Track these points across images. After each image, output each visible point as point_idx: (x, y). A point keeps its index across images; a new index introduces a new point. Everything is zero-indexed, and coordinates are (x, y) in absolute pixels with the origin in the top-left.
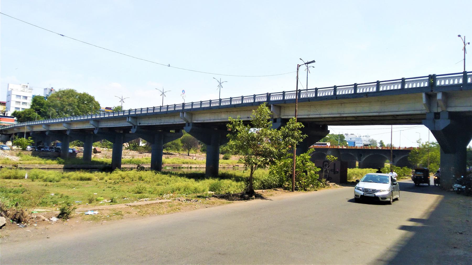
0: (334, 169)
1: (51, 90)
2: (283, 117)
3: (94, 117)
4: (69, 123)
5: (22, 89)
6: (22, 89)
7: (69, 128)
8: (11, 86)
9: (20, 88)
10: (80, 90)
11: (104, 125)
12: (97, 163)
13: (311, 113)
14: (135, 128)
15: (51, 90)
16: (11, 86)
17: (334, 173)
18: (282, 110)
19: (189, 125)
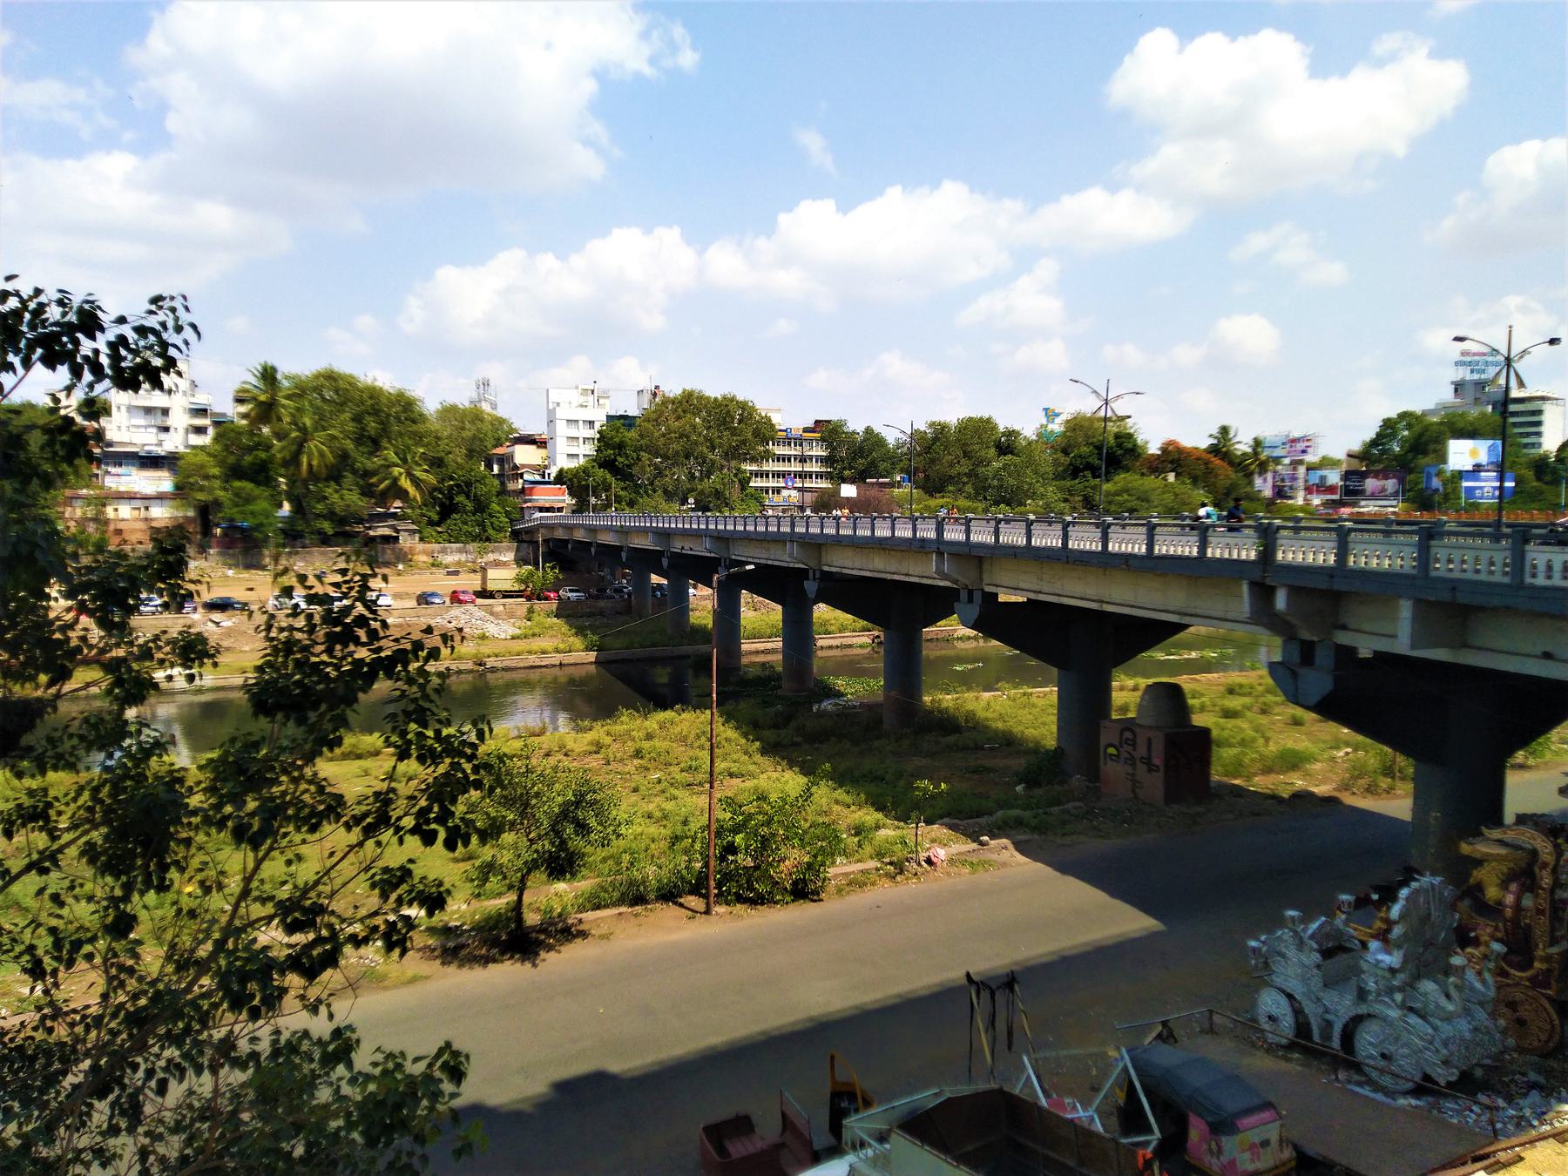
0: (1149, 758)
1: (655, 395)
2: (826, 568)
3: (954, 534)
4: (624, 531)
5: (582, 399)
6: (582, 399)
7: (813, 564)
8: (554, 396)
9: (576, 397)
10: (714, 390)
11: (677, 546)
12: (717, 614)
13: (1045, 589)
14: (970, 600)
15: (655, 395)
16: (554, 396)
17: (1150, 770)
18: (986, 566)
19: (970, 600)
